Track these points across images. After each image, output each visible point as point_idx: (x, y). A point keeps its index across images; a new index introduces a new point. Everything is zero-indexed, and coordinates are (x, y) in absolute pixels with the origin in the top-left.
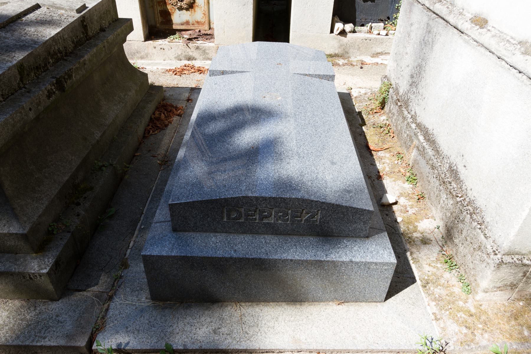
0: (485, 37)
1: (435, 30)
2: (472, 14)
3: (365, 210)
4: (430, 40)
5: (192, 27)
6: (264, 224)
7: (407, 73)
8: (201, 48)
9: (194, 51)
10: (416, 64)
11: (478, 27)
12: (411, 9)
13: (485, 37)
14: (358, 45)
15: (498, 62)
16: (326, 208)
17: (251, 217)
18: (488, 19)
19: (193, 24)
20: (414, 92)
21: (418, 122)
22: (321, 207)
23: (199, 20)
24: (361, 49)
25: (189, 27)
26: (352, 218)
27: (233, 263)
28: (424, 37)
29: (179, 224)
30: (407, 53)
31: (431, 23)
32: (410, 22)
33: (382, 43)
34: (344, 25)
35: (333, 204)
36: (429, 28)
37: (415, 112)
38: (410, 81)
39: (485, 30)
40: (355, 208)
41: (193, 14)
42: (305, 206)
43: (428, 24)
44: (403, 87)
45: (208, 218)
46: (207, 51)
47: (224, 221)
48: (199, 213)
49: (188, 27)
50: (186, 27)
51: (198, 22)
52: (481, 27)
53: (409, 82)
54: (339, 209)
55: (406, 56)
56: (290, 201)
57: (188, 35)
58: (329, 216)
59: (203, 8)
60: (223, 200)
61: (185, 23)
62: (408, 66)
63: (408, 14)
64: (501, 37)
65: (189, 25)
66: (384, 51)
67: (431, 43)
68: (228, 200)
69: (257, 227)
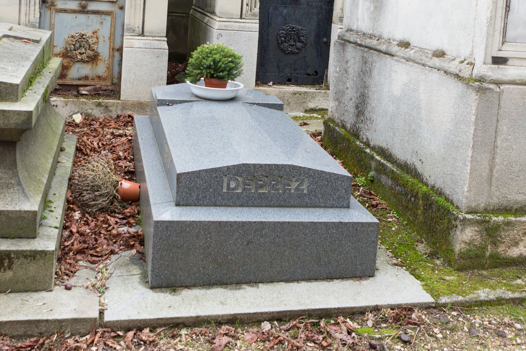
0: (410, 53)
1: (370, 59)
2: (397, 41)
3: (345, 176)
4: (368, 69)
5: (91, 83)
6: (260, 194)
7: (351, 107)
8: (103, 104)
9: (95, 108)
10: (359, 94)
11: (403, 48)
12: (344, 49)
13: (410, 53)
14: (287, 100)
15: (424, 68)
16: (313, 175)
17: (249, 187)
18: (410, 42)
19: (93, 79)
20: (362, 120)
21: (372, 146)
22: (308, 174)
23: (101, 75)
24: (291, 104)
25: (88, 82)
26: (334, 185)
27: (237, 228)
28: (362, 68)
29: (183, 196)
30: (347, 88)
31: (365, 55)
32: (346, 60)
33: (314, 97)
34: (118, 232)
35: (318, 170)
36: (365, 59)
37: (367, 138)
38: (356, 111)
39: (409, 49)
40: (336, 174)
41: (94, 68)
42: (295, 173)
43: (363, 57)
44: (349, 120)
45: (210, 188)
46: (110, 108)
47: (224, 192)
48: (203, 183)
49: (87, 82)
50: (84, 82)
51: (99, 77)
52: (407, 48)
53: (355, 113)
54: (323, 175)
55: (348, 91)
56: (282, 168)
57: (87, 91)
58: (315, 183)
59: (107, 62)
60: (226, 168)
61: (83, 78)
62: (351, 99)
63: (341, 54)
64: (422, 50)
65: (88, 80)
66: (317, 106)
67: (369, 72)
68: (229, 168)
69: (253, 199)
